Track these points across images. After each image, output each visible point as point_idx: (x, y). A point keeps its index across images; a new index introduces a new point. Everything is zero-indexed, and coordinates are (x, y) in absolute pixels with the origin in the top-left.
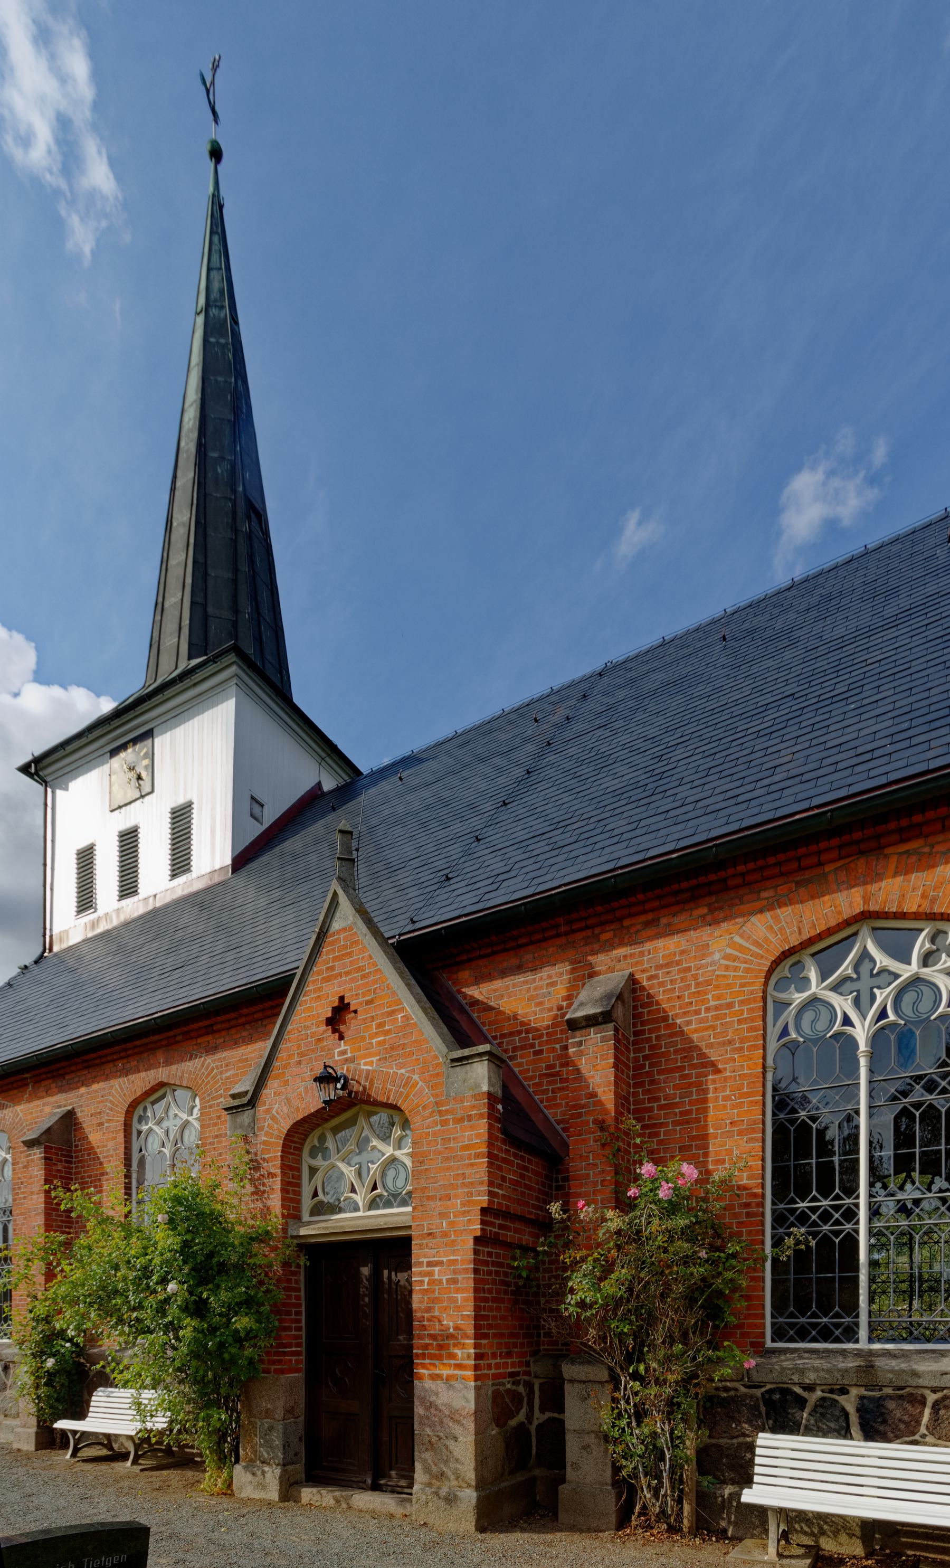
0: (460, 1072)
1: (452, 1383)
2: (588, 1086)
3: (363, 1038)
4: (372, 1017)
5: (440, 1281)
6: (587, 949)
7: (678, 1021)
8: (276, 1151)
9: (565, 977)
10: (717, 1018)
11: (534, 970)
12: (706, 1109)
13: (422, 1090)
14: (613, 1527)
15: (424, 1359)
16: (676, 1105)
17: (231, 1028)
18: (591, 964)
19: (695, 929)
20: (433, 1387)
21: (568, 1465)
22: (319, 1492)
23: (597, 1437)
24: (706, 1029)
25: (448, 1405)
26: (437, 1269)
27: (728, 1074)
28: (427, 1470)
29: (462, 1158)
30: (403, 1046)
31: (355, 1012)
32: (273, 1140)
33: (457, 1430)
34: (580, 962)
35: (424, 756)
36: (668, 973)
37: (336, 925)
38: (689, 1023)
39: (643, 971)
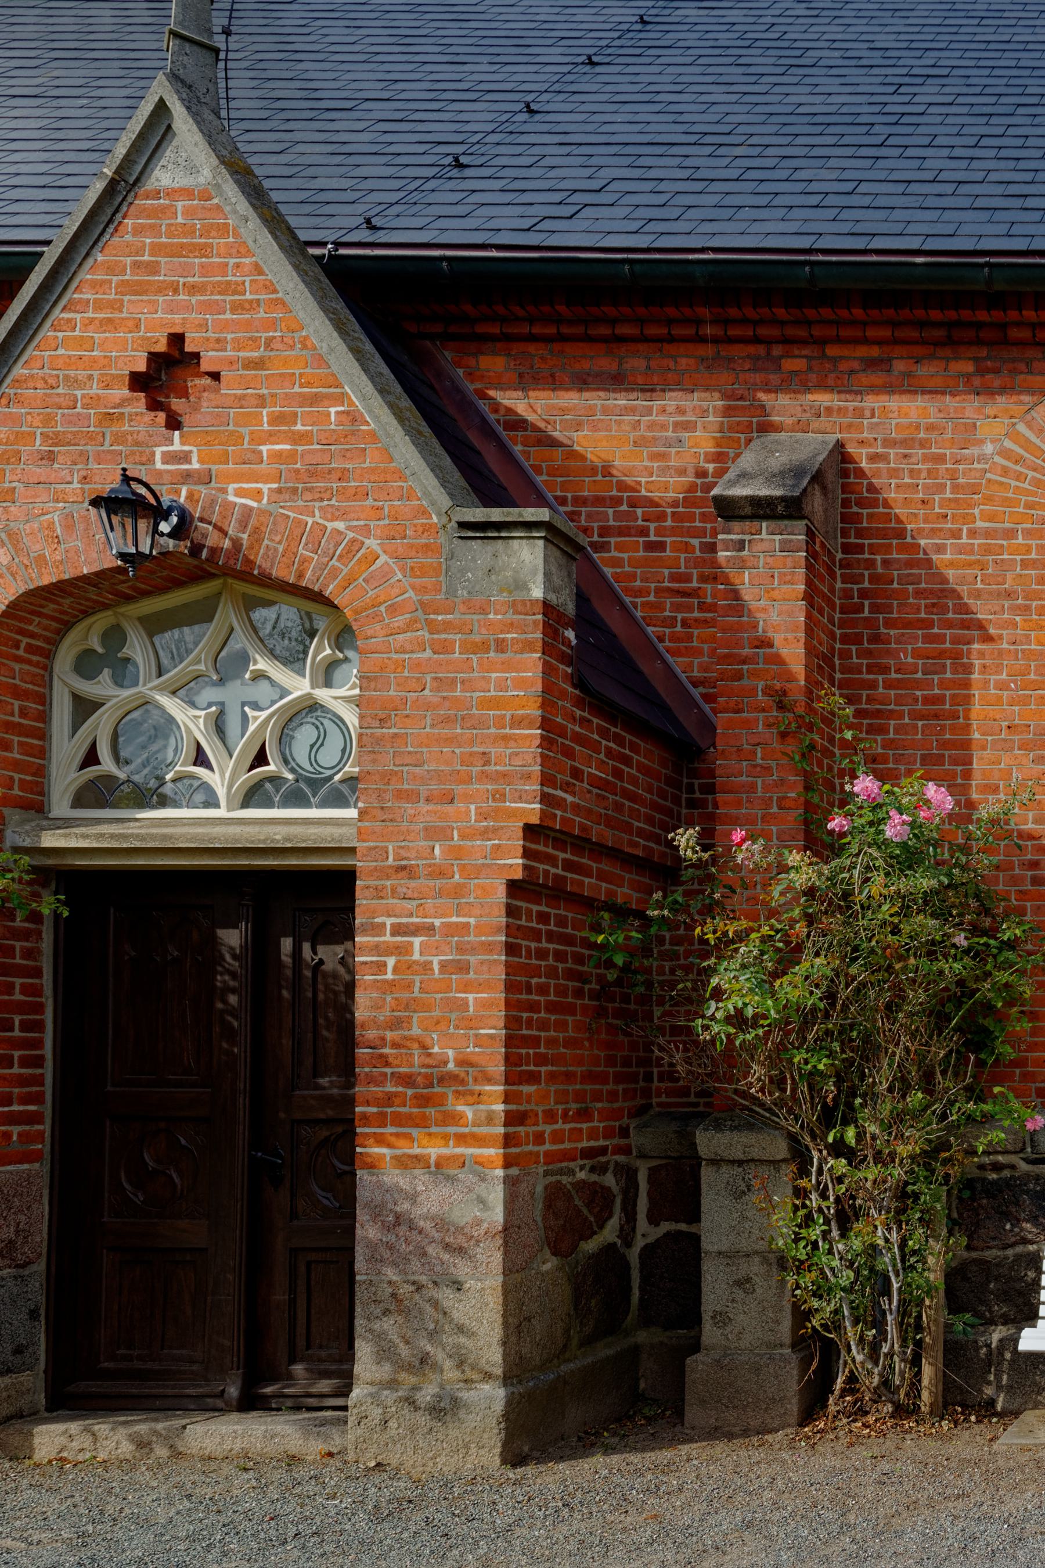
2: (755, 627)
4: (261, 397)
5: (427, 967)
6: (758, 377)
7: (922, 542)
9: (711, 418)
10: (987, 550)
11: (649, 389)
12: (967, 700)
13: (386, 574)
18: (763, 407)
19: (953, 395)
20: (403, 1183)
21: (706, 1317)
22: (86, 1430)
23: (765, 1261)
24: (970, 565)
26: (417, 941)
28: (385, 1352)
29: (482, 723)
31: (216, 376)
33: (462, 1269)
36: (905, 456)
38: (940, 549)
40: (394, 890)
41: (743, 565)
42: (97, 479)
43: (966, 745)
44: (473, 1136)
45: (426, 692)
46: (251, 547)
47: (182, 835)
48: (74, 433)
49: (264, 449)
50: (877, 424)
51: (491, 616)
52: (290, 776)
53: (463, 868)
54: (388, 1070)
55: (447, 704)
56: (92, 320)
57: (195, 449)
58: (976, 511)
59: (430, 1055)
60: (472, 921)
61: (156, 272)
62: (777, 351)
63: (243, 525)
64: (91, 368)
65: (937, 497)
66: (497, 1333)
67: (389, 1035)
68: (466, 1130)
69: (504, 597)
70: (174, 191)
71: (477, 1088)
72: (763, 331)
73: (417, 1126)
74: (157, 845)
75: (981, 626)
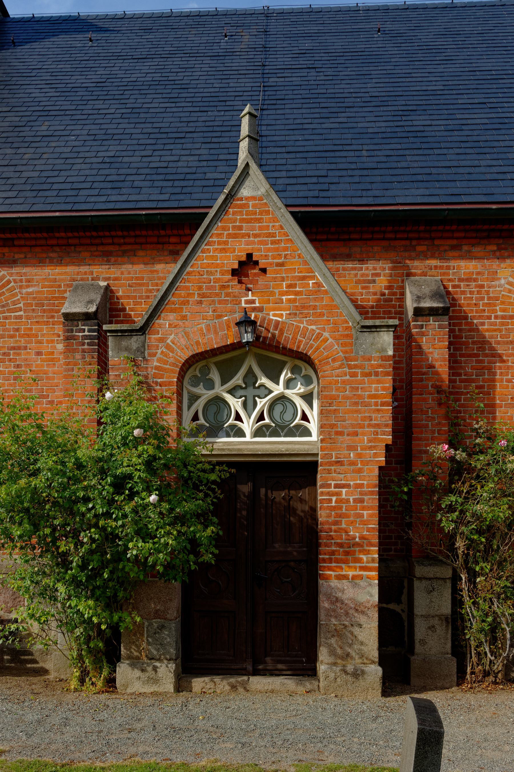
0: (368, 338)
1: (357, 581)
2: (428, 360)
3: (273, 294)
4: (283, 277)
5: (348, 501)
6: (406, 254)
7: (475, 321)
8: (174, 378)
9: (387, 271)
10: (503, 324)
11: (362, 261)
12: (494, 387)
13: (332, 345)
14: (455, 684)
15: (331, 563)
16: (473, 381)
17: (36, 246)
18: (408, 266)
19: (488, 259)
20: (339, 586)
21: (417, 642)
22: (212, 680)
23: (440, 619)
24: (495, 330)
25: (352, 599)
26: (344, 490)
27: (510, 364)
28: (332, 653)
30: (315, 307)
31: (264, 271)
32: (168, 366)
33: (362, 619)
34: (400, 263)
35: (100, 24)
36: (468, 285)
37: (245, 192)
38: (483, 324)
39: (450, 280)
40: (335, 471)
41: (423, 334)
42: (219, 310)
43: (494, 406)
44: (366, 567)
45: (347, 392)
46: (279, 336)
47: (246, 449)
48: (210, 293)
49: (284, 298)
50: (456, 272)
51: (373, 362)
52: (274, 425)
53: (362, 462)
54: (333, 541)
55: (355, 397)
56: (217, 249)
57: (257, 298)
58: (498, 308)
59: (349, 535)
60: (365, 482)
61: (242, 230)
62: (414, 243)
63: (276, 328)
64: (217, 267)
65: (481, 302)
66: (376, 645)
67: (333, 527)
68: (364, 565)
69: (378, 354)
70: (249, 197)
71: (368, 548)
72: (412, 235)
73: (344, 563)
74: (229, 453)
75: (500, 356)
